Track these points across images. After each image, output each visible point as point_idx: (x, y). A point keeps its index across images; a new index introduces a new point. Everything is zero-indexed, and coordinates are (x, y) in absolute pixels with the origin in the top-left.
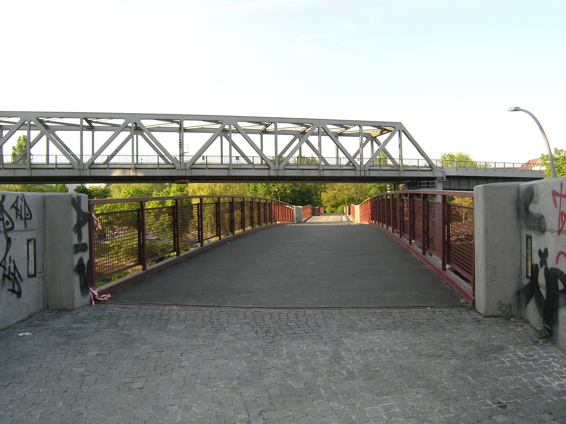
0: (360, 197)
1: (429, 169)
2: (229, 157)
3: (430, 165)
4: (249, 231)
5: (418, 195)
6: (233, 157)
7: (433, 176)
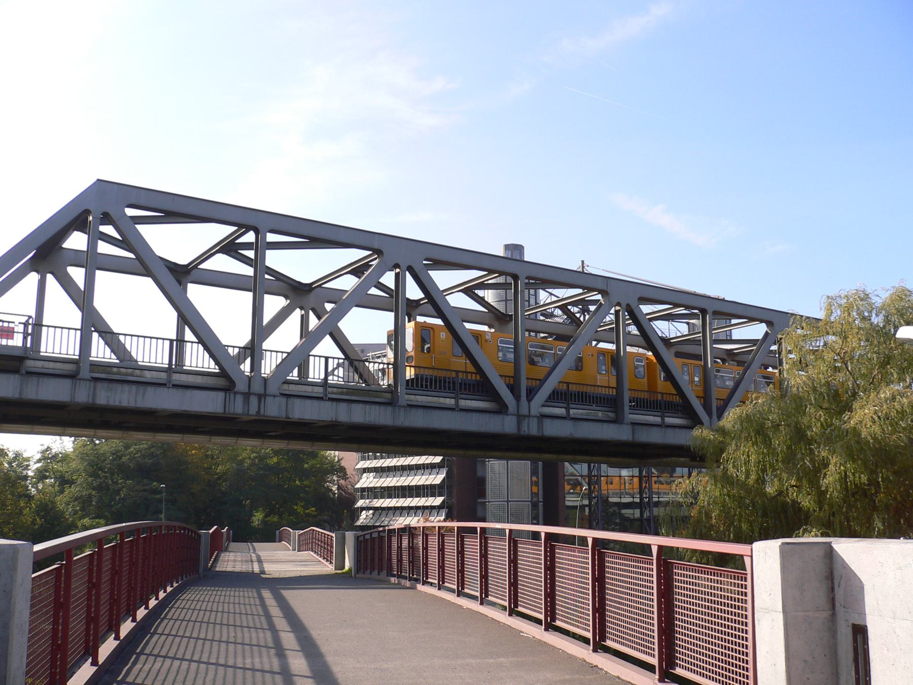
0: (30, 484)
1: (221, 382)
2: (79, 333)
3: (221, 367)
4: (145, 617)
5: (473, 530)
6: (268, 353)
7: (108, 402)
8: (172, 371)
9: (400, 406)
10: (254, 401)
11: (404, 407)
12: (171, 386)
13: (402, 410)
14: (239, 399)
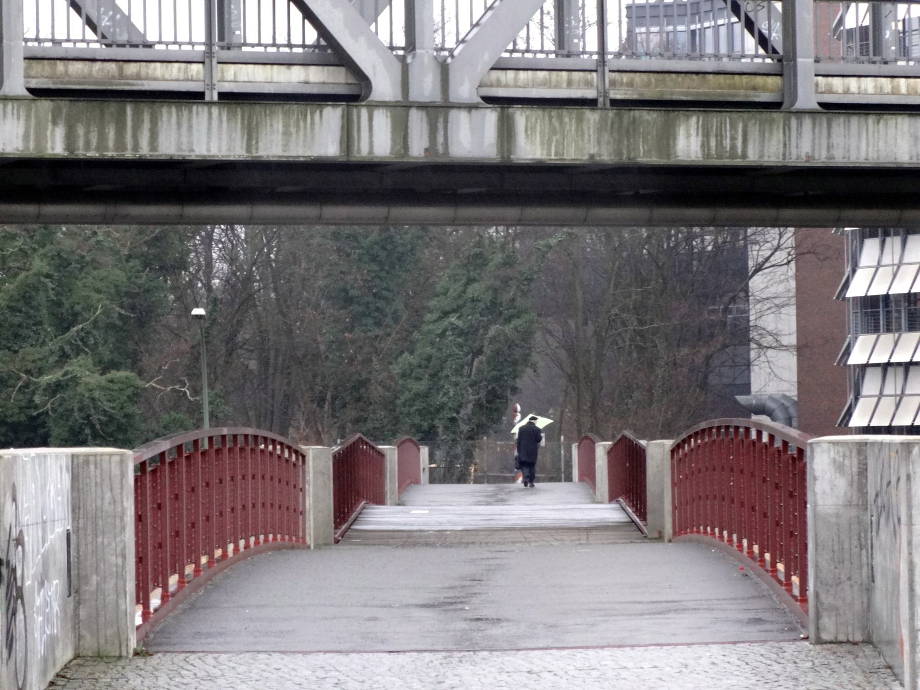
8: (214, 61)
9: (801, 113)
10: (417, 122)
11: (811, 113)
12: (215, 98)
13: (807, 122)
14: (382, 122)
